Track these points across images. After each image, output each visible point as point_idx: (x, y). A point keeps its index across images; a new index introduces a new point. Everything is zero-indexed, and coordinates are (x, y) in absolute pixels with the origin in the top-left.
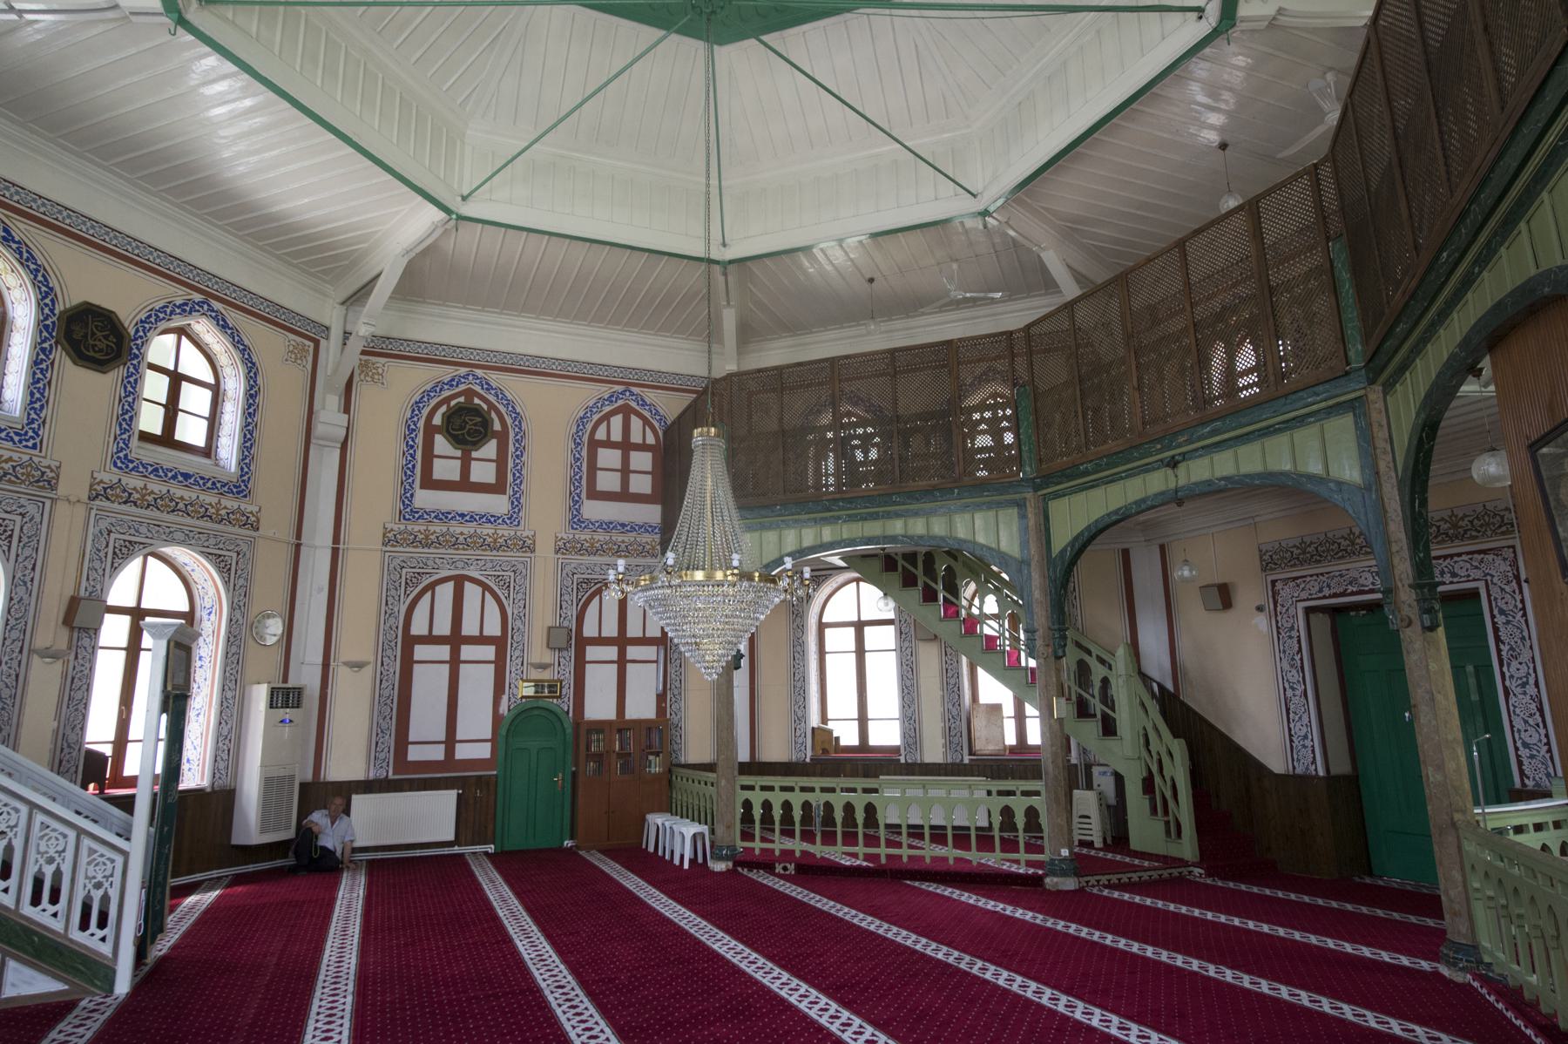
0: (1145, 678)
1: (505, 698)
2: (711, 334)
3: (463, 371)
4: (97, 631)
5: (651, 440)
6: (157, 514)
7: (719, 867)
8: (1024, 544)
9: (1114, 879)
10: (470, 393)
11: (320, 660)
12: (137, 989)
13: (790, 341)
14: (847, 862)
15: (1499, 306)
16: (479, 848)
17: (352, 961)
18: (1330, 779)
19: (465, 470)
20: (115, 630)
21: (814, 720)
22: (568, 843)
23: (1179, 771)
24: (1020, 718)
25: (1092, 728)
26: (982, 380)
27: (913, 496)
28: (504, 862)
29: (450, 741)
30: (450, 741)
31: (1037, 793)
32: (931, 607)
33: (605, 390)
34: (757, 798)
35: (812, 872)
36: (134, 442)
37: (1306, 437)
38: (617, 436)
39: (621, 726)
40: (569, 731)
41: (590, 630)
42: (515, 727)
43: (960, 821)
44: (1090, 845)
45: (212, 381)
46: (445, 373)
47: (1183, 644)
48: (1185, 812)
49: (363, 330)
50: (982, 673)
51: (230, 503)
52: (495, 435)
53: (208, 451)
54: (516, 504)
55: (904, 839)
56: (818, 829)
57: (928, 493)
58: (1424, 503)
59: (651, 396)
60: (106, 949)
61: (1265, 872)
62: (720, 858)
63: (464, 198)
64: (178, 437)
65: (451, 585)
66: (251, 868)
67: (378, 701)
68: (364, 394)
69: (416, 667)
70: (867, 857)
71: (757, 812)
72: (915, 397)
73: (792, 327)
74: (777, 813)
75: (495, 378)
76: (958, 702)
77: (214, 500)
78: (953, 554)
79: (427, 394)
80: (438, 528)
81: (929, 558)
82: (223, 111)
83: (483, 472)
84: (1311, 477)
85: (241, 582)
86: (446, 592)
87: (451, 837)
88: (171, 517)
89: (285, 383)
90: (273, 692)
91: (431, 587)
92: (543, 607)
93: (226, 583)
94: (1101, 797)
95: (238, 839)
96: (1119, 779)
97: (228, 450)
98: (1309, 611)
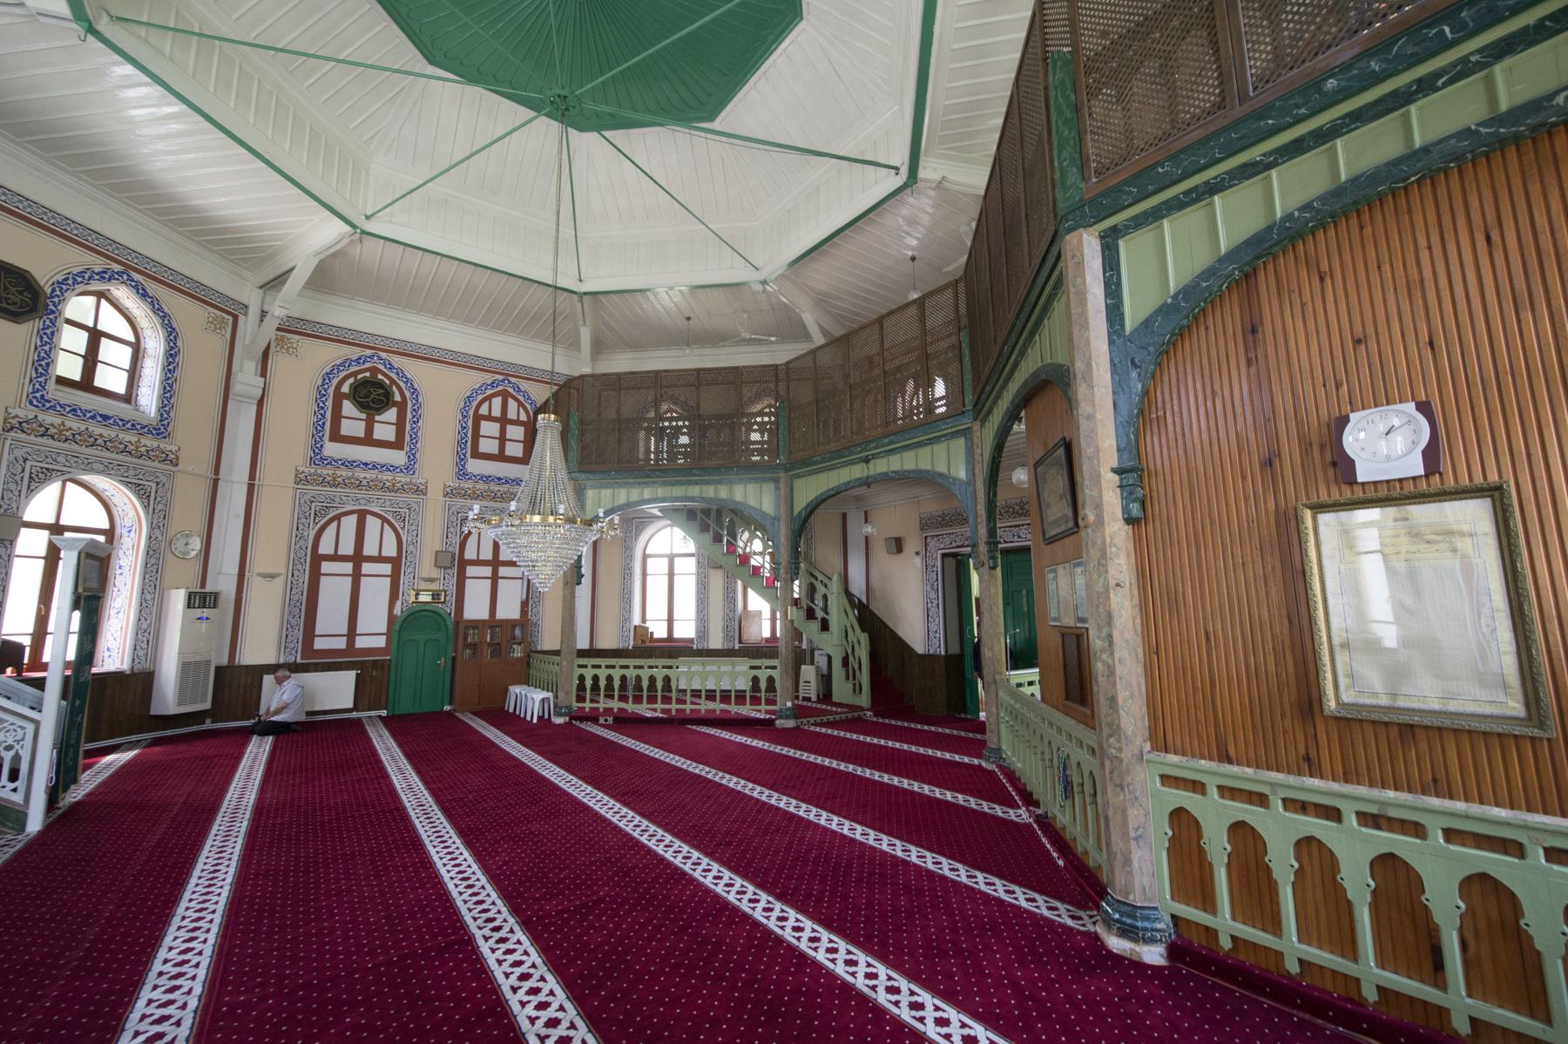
0: (849, 595)
1: (398, 604)
2: (575, 345)
3: (369, 352)
4: (12, 542)
5: (523, 417)
6: (76, 447)
7: (559, 720)
8: (777, 506)
9: (818, 720)
10: (374, 371)
11: (236, 571)
12: (48, 829)
13: (632, 355)
14: (649, 714)
15: (1026, 382)
16: (373, 713)
17: (251, 797)
18: (948, 658)
19: (369, 429)
20: (31, 543)
21: (637, 620)
22: (447, 708)
23: (863, 653)
24: (773, 619)
25: (814, 626)
26: (758, 397)
27: (706, 470)
28: (398, 725)
29: (352, 633)
30: (352, 633)
31: (774, 668)
32: (718, 546)
33: (488, 378)
34: (589, 674)
35: (624, 722)
36: (51, 385)
37: (940, 449)
38: (497, 412)
39: (493, 624)
40: (451, 627)
41: (470, 554)
42: (406, 625)
43: (725, 686)
44: (809, 699)
45: (132, 339)
46: (355, 353)
47: (874, 573)
48: (865, 678)
49: (278, 311)
50: (750, 592)
51: (150, 442)
52: (395, 404)
53: (129, 398)
54: (412, 458)
55: (688, 699)
56: (630, 694)
57: (717, 470)
58: (995, 494)
59: (524, 385)
60: (18, 798)
61: (908, 713)
62: (558, 714)
63: (368, 218)
64: (97, 383)
65: (355, 517)
66: (169, 733)
67: (289, 602)
68: (278, 362)
69: (323, 579)
70: (663, 711)
71: (589, 683)
72: (712, 402)
73: (633, 345)
74: (602, 683)
75: (396, 360)
76: (734, 609)
77: (134, 439)
78: (734, 511)
79: (338, 368)
80: (344, 473)
81: (719, 513)
82: (141, 115)
83: (385, 432)
84: (941, 475)
85: (160, 507)
86: (350, 523)
87: (351, 705)
88: (90, 451)
89: (204, 347)
90: (190, 596)
91: (338, 518)
92: (431, 537)
93: (146, 507)
94: (818, 669)
95: (156, 709)
96: (830, 658)
97: (148, 398)
98: (944, 555)
